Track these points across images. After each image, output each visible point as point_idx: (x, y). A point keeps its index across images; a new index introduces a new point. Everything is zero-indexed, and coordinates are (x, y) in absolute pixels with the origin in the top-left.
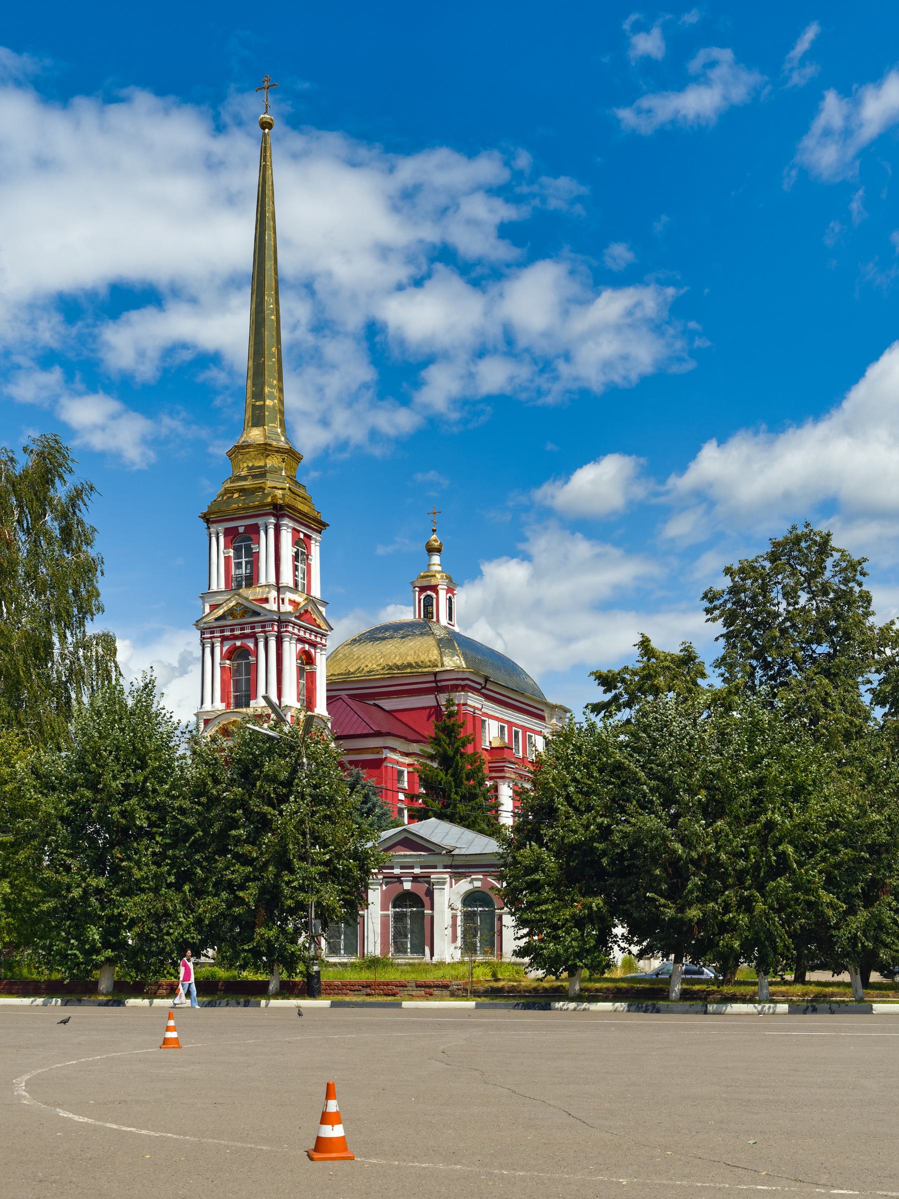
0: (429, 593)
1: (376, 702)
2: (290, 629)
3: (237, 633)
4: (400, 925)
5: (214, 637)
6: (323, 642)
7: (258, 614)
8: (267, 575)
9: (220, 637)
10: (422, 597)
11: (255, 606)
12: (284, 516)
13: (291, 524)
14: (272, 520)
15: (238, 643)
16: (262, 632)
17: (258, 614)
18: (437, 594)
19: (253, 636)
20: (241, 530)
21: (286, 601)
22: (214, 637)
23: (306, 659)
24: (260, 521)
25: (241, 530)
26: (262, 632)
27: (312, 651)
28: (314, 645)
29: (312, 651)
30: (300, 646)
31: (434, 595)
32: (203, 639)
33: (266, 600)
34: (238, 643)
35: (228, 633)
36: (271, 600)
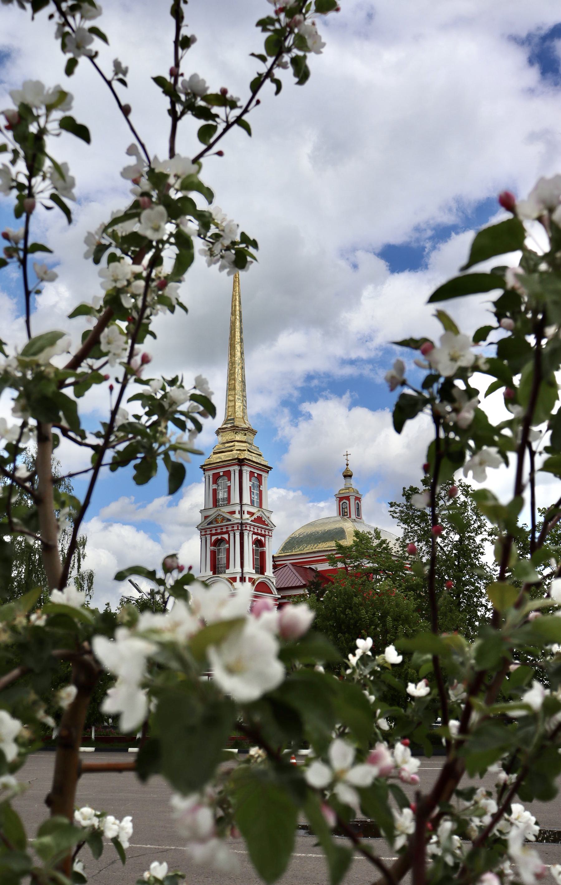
0: (344, 501)
1: (311, 566)
2: (248, 528)
3: (219, 531)
4: (127, 574)
5: (206, 534)
6: (270, 534)
7: (230, 520)
8: (235, 499)
9: (210, 534)
10: (341, 503)
11: (228, 516)
12: (244, 465)
13: (250, 469)
14: (237, 468)
15: (219, 537)
16: (232, 530)
17: (230, 520)
18: (349, 500)
19: (227, 532)
20: (221, 474)
21: (246, 513)
22: (206, 534)
23: (259, 544)
24: (231, 469)
25: (221, 474)
26: (232, 530)
27: (263, 539)
28: (264, 536)
29: (263, 539)
30: (255, 537)
31: (347, 502)
32: (201, 535)
33: (234, 512)
34: (219, 537)
35: (214, 532)
36: (237, 512)
